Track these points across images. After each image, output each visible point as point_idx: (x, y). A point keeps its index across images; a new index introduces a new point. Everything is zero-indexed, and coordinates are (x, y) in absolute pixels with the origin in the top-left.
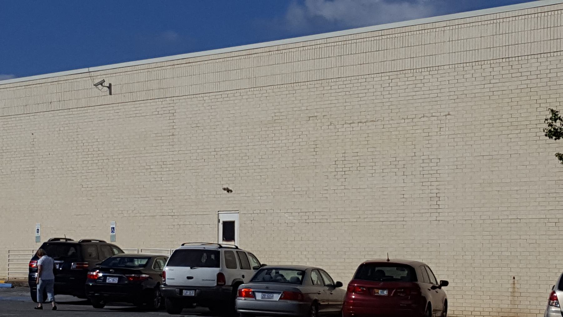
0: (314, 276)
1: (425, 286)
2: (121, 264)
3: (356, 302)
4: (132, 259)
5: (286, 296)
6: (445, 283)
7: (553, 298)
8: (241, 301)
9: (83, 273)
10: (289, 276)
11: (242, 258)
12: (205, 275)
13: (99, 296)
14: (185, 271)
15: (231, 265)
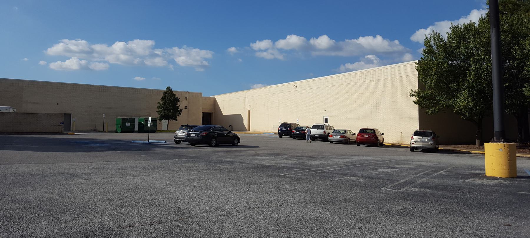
0: (348, 132)
1: (378, 134)
2: (300, 129)
3: (359, 139)
4: (302, 127)
5: (341, 137)
6: (383, 134)
7: (412, 138)
8: (330, 138)
9: (291, 130)
10: (342, 132)
11: (330, 127)
12: (321, 132)
13: (294, 137)
14: (316, 130)
15: (327, 129)
